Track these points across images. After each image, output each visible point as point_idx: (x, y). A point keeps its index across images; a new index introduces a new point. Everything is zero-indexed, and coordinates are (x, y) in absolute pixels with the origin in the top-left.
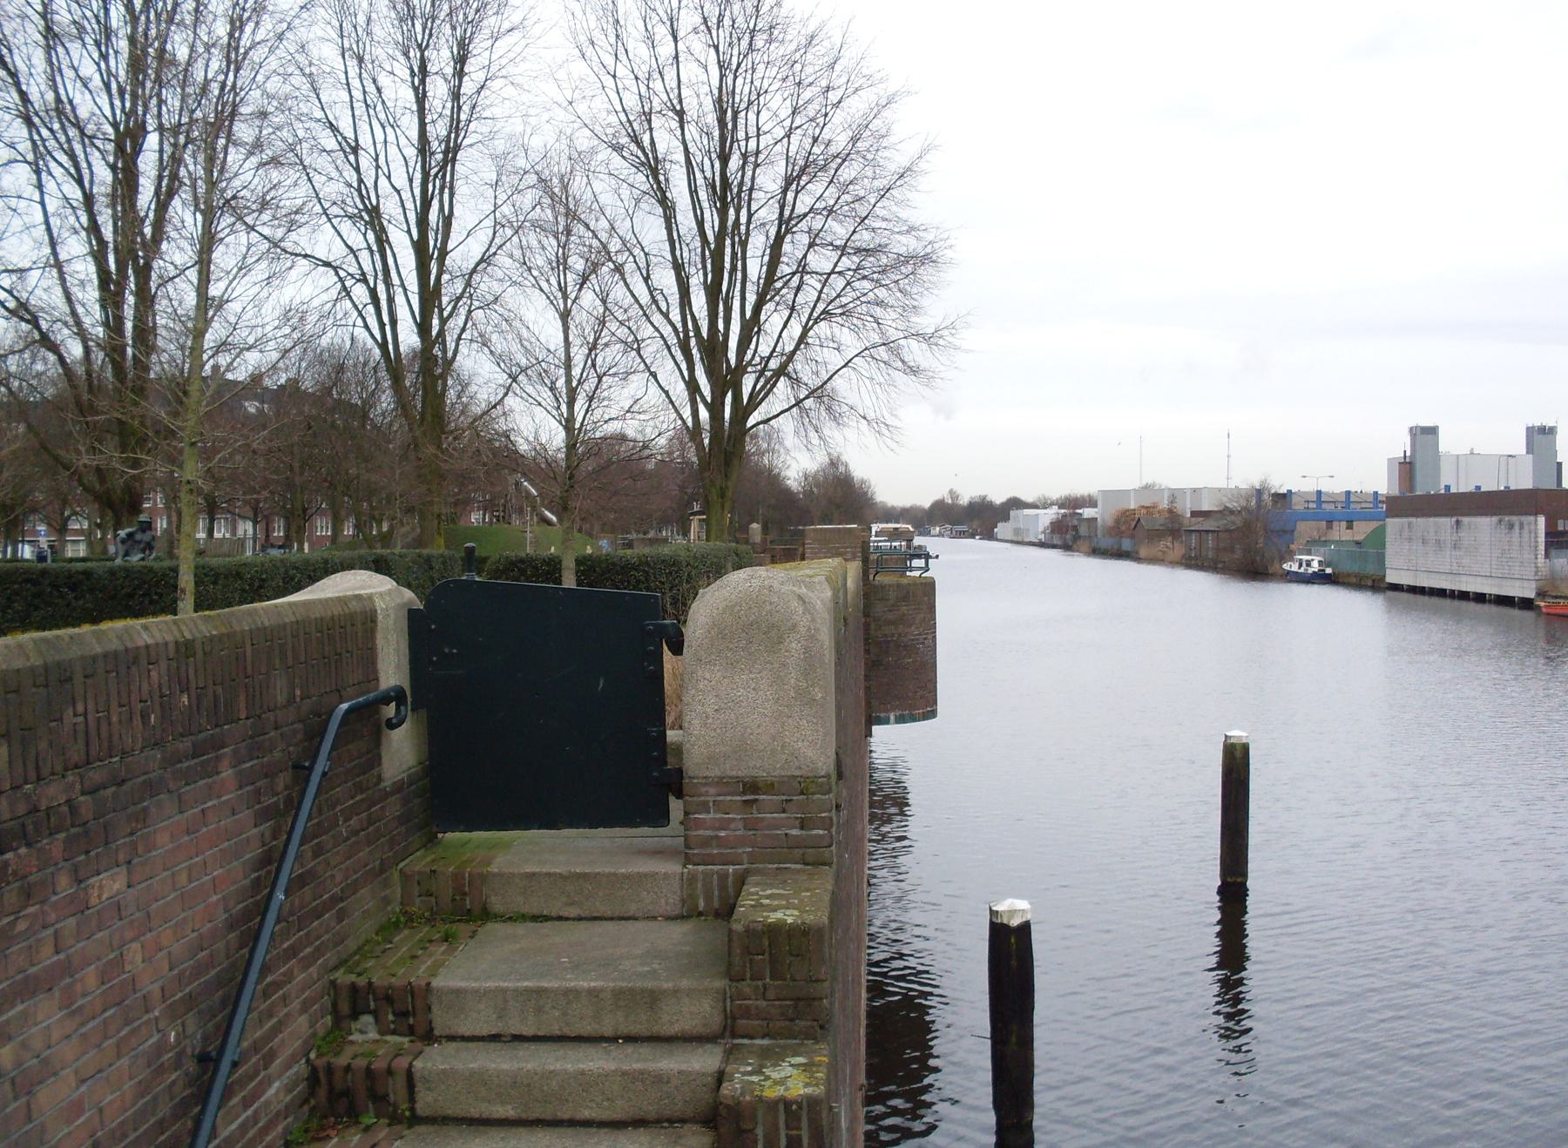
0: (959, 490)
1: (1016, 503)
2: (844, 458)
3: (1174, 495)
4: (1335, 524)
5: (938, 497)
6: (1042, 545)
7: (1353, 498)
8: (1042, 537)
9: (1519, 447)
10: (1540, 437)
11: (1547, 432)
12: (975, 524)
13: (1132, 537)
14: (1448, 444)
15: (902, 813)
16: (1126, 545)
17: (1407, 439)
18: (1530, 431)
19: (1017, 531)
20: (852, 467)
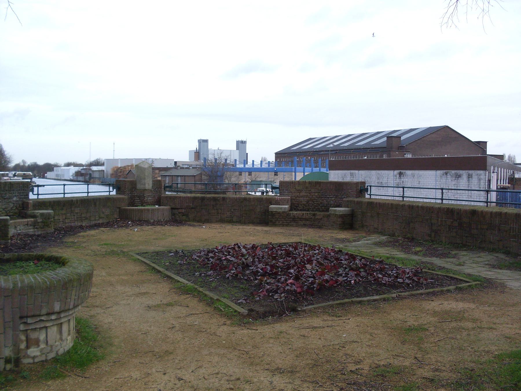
1: (56, 166)
3: (153, 161)
4: (243, 174)
6: (71, 180)
7: (178, 164)
8: (72, 178)
9: (234, 147)
10: (241, 144)
11: (244, 143)
14: (212, 146)
15: (99, 333)
17: (197, 144)
18: (238, 142)
19: (57, 175)
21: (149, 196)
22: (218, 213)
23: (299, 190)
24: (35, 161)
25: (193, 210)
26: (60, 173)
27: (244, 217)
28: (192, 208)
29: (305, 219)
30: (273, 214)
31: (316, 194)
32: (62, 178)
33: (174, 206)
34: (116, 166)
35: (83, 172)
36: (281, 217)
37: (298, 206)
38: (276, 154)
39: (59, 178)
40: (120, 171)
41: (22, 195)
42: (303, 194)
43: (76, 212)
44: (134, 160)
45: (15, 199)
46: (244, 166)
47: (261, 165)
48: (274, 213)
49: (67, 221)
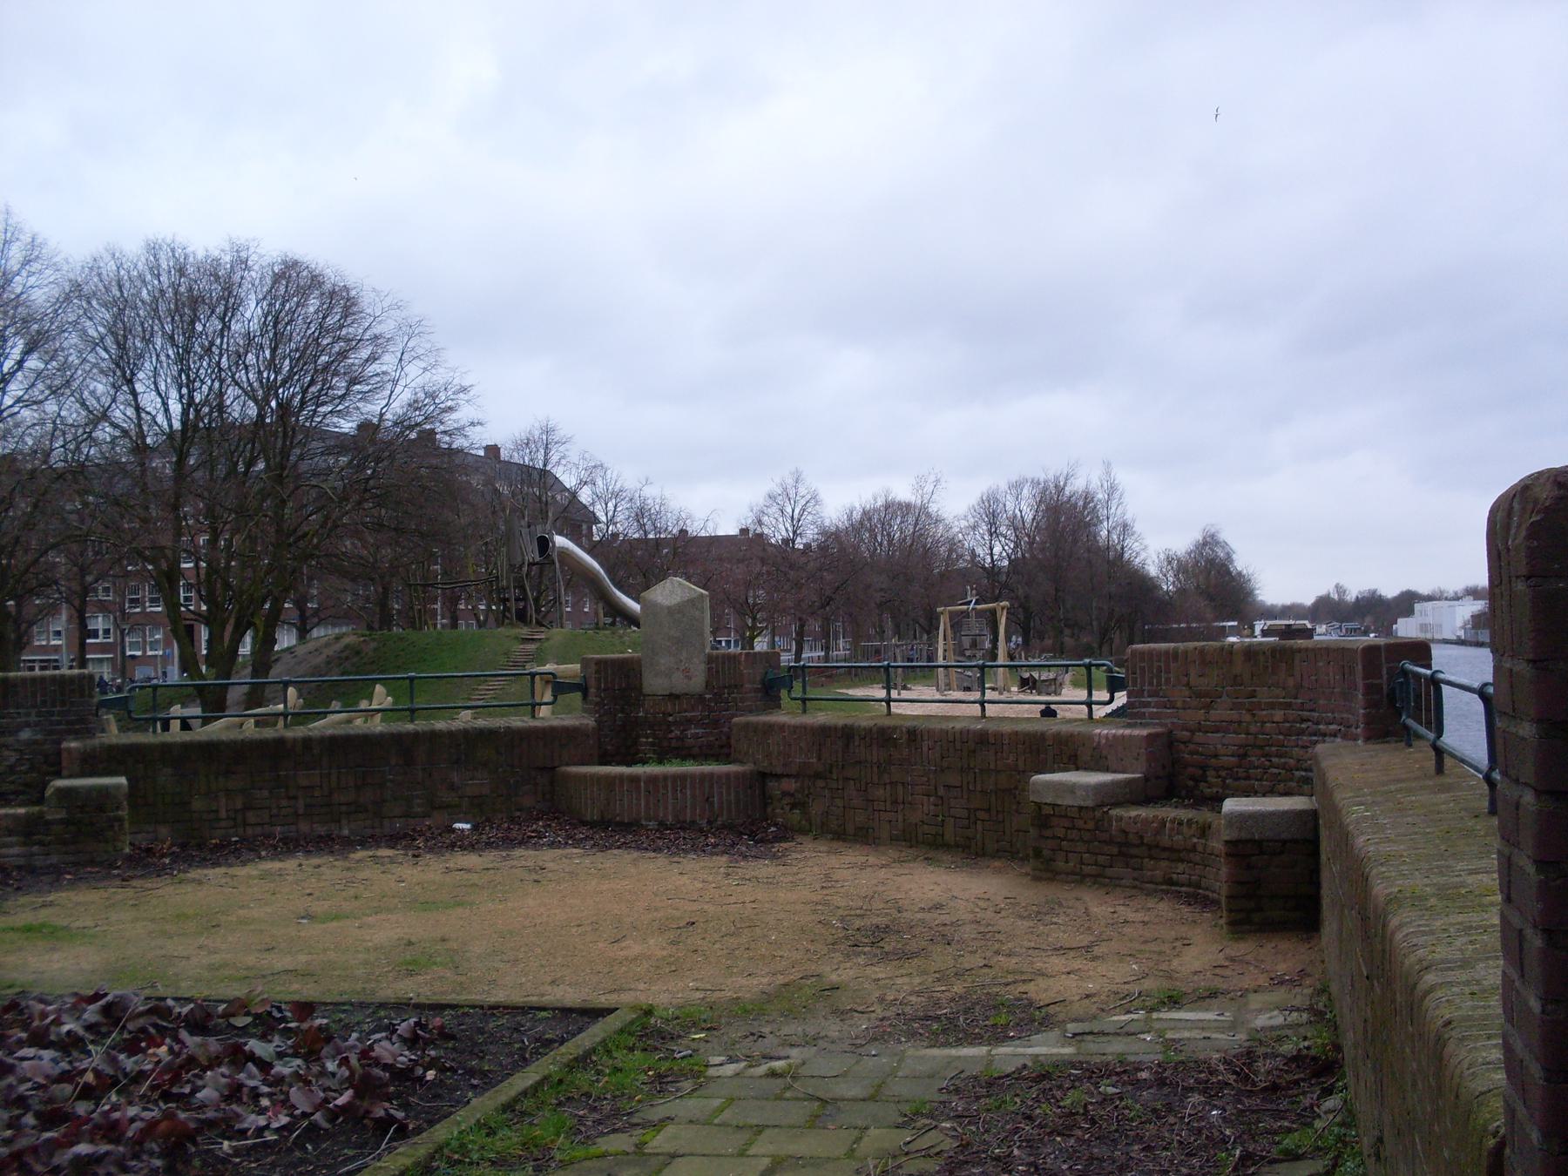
5: (1322, 592)
6: (1460, 642)
8: (1461, 633)
12: (1368, 620)
21: (689, 721)
22: (895, 802)
23: (1207, 695)
25: (820, 783)
26: (1430, 620)
27: (979, 825)
28: (818, 776)
29: (1170, 849)
30: (1045, 817)
31: (1278, 715)
36: (1074, 834)
37: (1204, 779)
41: (59, 723)
42: (1221, 713)
43: (304, 782)
45: (25, 735)
48: (1048, 810)
49: (251, 817)
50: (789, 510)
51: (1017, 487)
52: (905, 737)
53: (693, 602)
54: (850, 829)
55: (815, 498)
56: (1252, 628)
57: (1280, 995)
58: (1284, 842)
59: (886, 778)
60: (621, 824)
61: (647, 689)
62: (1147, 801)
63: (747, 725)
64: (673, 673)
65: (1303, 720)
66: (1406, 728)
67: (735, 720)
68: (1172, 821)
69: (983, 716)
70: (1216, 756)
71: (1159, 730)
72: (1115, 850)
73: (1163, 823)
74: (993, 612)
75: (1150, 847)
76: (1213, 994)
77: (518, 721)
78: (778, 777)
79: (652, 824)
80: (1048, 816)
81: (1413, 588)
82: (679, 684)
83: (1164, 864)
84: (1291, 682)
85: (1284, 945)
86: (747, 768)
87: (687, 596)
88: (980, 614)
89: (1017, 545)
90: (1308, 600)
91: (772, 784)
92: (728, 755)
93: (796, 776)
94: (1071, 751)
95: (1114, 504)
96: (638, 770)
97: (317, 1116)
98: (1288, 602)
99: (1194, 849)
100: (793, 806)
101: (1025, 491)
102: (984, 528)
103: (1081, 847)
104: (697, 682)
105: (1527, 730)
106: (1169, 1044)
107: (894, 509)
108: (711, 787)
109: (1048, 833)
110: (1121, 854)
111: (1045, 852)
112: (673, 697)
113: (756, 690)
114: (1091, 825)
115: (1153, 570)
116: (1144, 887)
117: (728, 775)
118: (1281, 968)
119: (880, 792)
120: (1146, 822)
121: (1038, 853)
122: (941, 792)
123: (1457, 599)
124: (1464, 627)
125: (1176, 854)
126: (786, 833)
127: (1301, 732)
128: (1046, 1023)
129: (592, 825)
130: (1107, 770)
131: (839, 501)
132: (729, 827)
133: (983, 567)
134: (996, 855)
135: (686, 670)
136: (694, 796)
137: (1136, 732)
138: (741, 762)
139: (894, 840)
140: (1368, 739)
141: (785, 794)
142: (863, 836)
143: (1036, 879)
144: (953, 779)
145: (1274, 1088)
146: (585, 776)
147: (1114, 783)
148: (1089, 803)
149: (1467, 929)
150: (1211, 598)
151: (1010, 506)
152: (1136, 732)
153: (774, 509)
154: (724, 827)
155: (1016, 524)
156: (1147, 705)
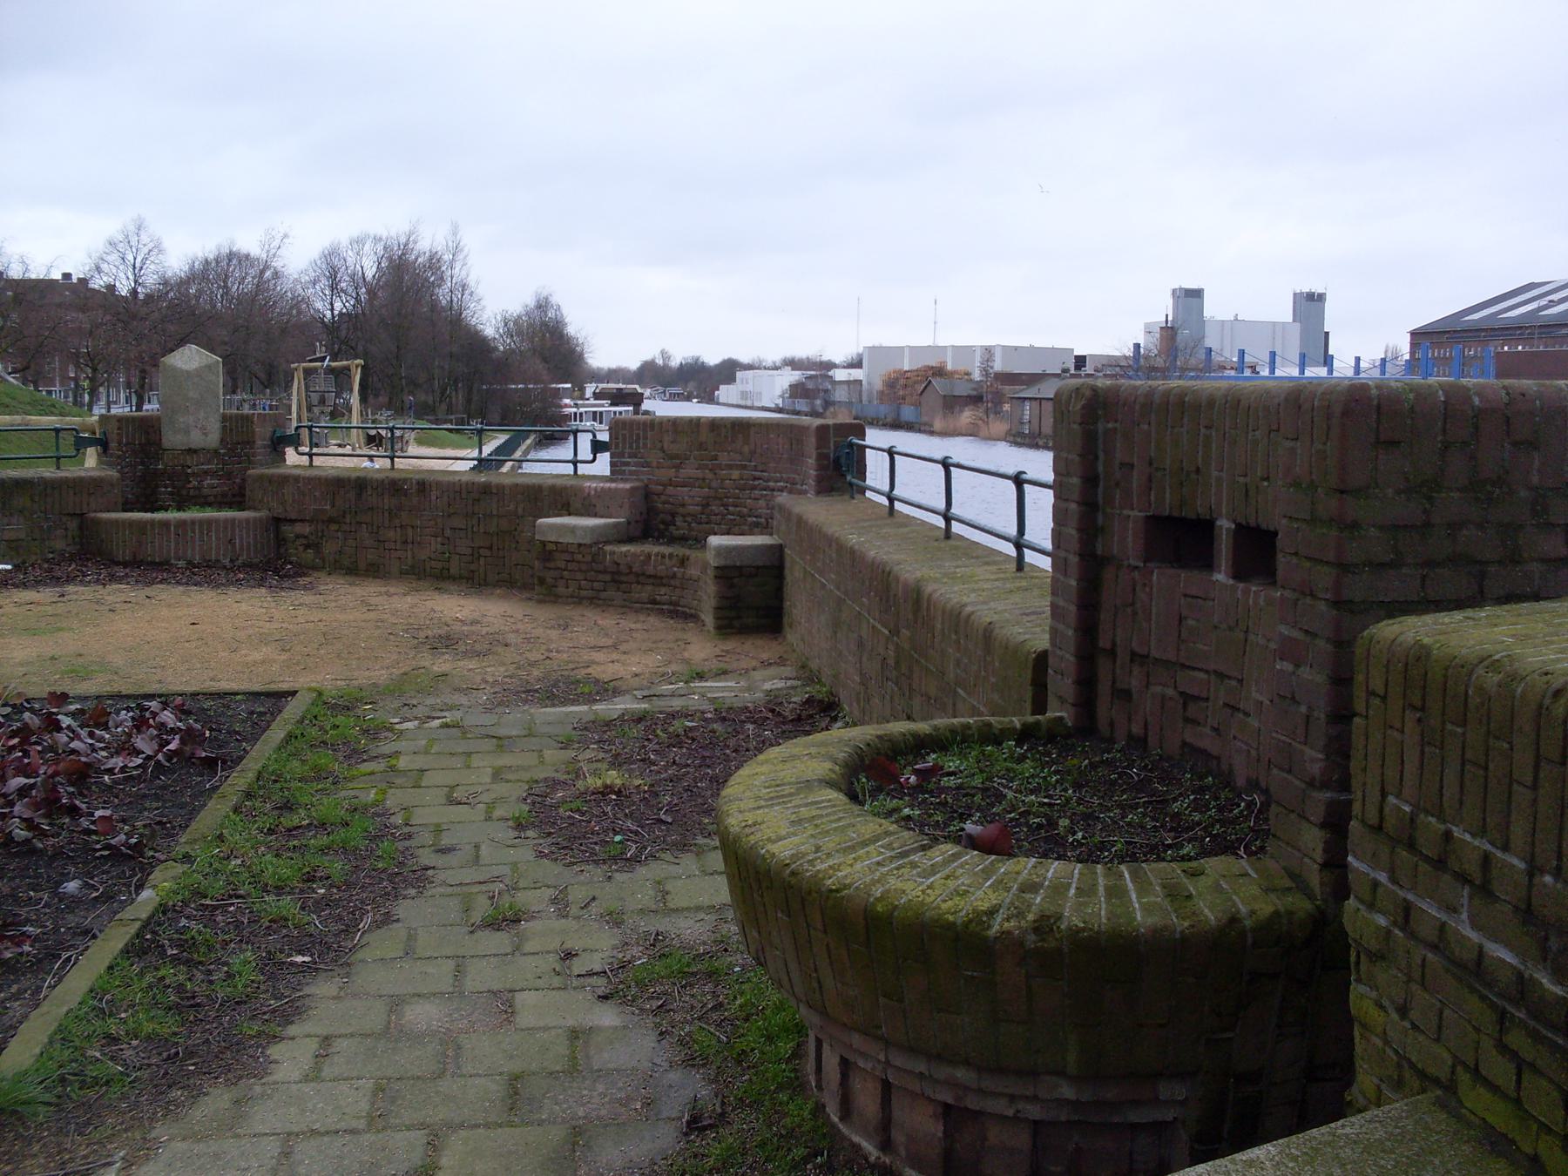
0: (672, 351)
2: (554, 300)
5: (648, 357)
8: (780, 402)
9: (1285, 313)
10: (1310, 304)
12: (691, 386)
13: (918, 405)
14: (1214, 309)
16: (908, 413)
17: (1170, 302)
19: (744, 395)
20: (565, 311)
21: (206, 472)
22: (406, 542)
23: (677, 457)
24: (696, 354)
25: (334, 527)
26: (749, 388)
27: (482, 561)
28: (331, 520)
29: (654, 577)
30: (548, 552)
31: (736, 474)
32: (757, 404)
33: (279, 511)
34: (898, 367)
35: (810, 385)
38: (1414, 334)
39: (749, 403)
40: (902, 381)
42: (689, 471)
44: (949, 354)
46: (1302, 372)
47: (1383, 372)
48: (551, 547)
50: (130, 257)
51: (359, 242)
52: (415, 487)
53: (209, 367)
54: (362, 565)
55: (158, 248)
56: (582, 390)
57: (771, 671)
58: (758, 568)
59: (397, 522)
60: (153, 563)
61: (166, 444)
62: (630, 540)
63: (261, 477)
64: (197, 430)
65: (755, 479)
66: (851, 484)
67: (250, 472)
68: (657, 555)
69: (393, 468)
70: (683, 505)
71: (637, 484)
72: (608, 578)
73: (649, 556)
74: (348, 368)
75: (637, 575)
76: (725, 672)
77: (47, 472)
78: (292, 521)
79: (181, 563)
80: (550, 552)
81: (734, 357)
82: (196, 439)
83: (649, 588)
84: (746, 449)
85: (759, 642)
86: (263, 514)
87: (205, 362)
88: (330, 370)
89: (357, 299)
90: (633, 364)
91: (286, 528)
92: (240, 503)
93: (311, 521)
94: (562, 497)
95: (458, 266)
96: (159, 516)
97: (160, 756)
98: (613, 366)
99: (674, 576)
100: (307, 547)
101: (367, 247)
102: (324, 282)
103: (579, 576)
104: (213, 438)
105: (1075, 480)
106: (713, 700)
107: (235, 258)
108: (233, 531)
109: (552, 565)
110: (614, 581)
111: (549, 580)
112: (191, 451)
113: (265, 447)
114: (589, 558)
115: (489, 332)
116: (629, 606)
117: (247, 520)
118: (765, 656)
119: (391, 534)
120: (634, 555)
121: (542, 581)
122: (448, 532)
123: (776, 368)
124: (782, 396)
125: (658, 580)
126: (301, 570)
127: (754, 488)
128: (617, 692)
129: (125, 565)
130: (595, 515)
131: (179, 251)
132: (249, 566)
133: (323, 322)
134: (498, 584)
135: (203, 428)
136: (218, 539)
137: (621, 486)
138: (255, 509)
139: (403, 574)
140: (818, 493)
141: (298, 537)
142: (374, 571)
143: (540, 602)
144: (457, 522)
145: (799, 719)
146: (117, 521)
147: (606, 525)
148: (587, 541)
149: (974, 591)
150: (545, 360)
151: (351, 261)
152: (621, 486)
153: (114, 257)
154: (245, 565)
155: (357, 280)
156: (628, 464)
